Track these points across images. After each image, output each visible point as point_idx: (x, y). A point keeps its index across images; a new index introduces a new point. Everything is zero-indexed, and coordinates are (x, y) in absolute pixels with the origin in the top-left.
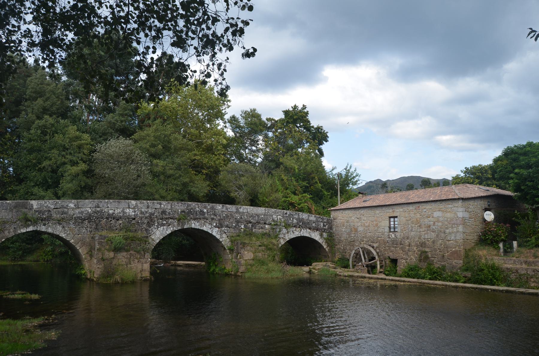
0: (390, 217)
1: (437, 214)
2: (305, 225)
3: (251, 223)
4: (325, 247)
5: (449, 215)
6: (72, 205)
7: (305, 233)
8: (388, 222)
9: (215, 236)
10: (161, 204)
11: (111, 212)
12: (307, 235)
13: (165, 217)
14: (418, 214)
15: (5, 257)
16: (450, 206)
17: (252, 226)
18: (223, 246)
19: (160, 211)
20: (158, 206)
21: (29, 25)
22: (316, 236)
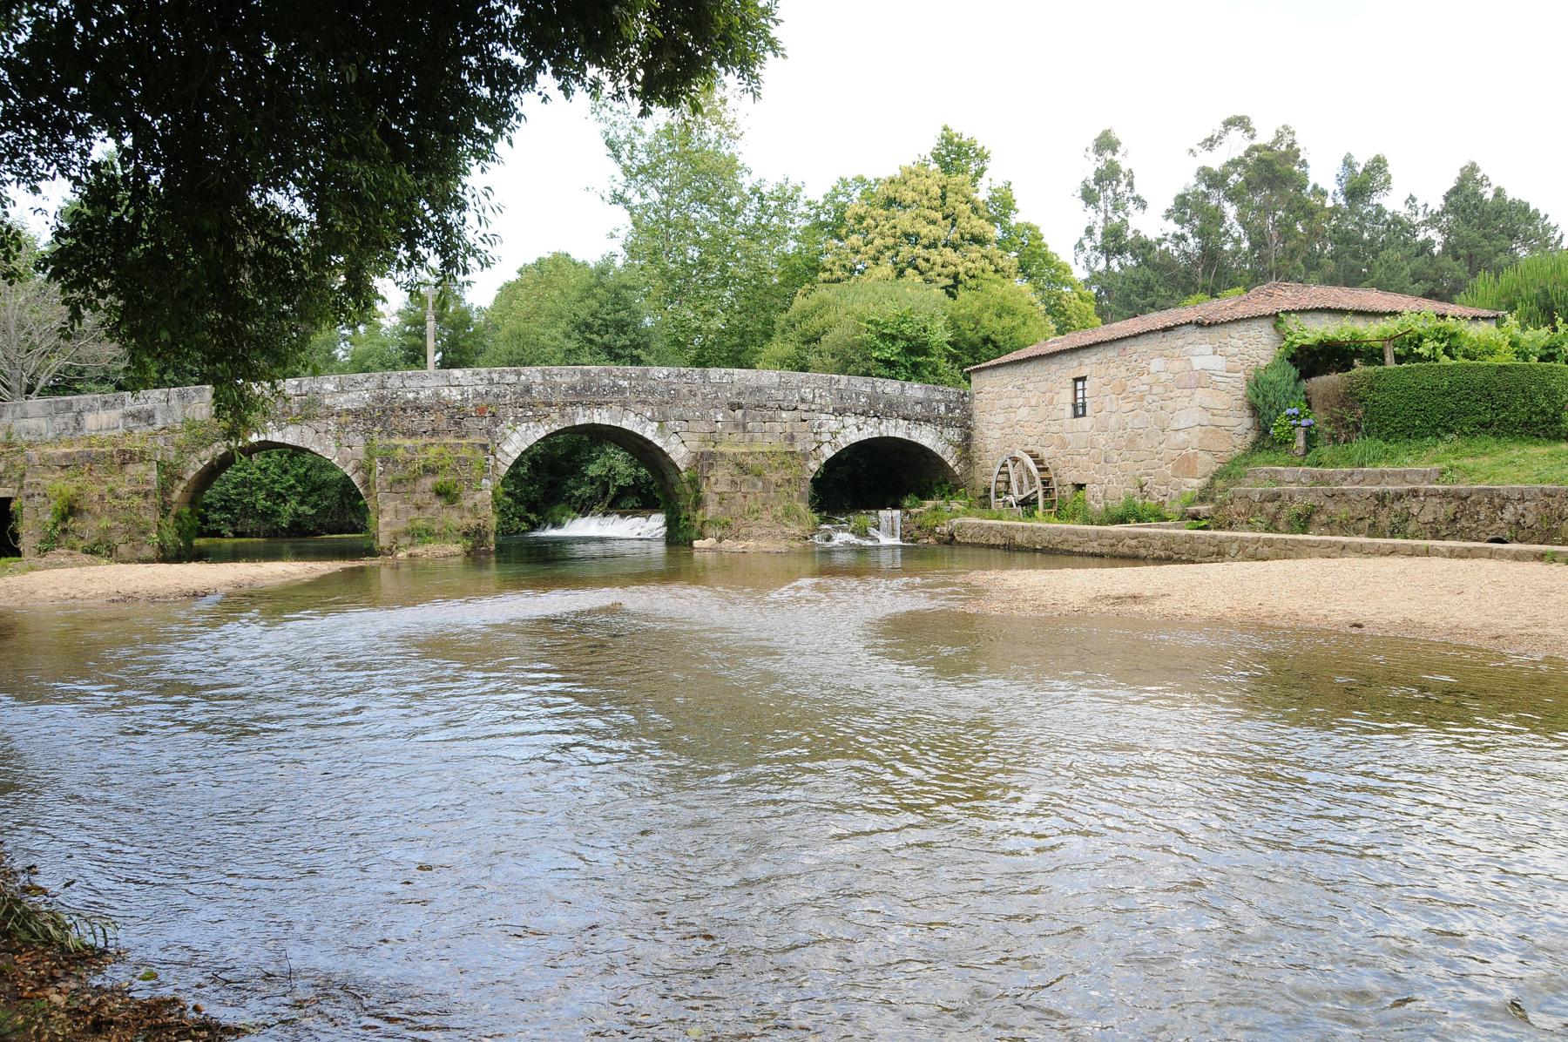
0: (1076, 380)
1: (1156, 364)
2: (891, 409)
3: (740, 407)
4: (951, 464)
5: (1176, 365)
6: (330, 387)
7: (895, 429)
8: (1070, 392)
9: (650, 442)
10: (519, 374)
11: (411, 396)
12: (900, 434)
13: (527, 404)
14: (1123, 369)
15: (663, 625)
16: (1180, 342)
17: (744, 415)
18: (674, 465)
19: (519, 388)
20: (512, 378)
21: (35, 419)
22: (926, 437)
